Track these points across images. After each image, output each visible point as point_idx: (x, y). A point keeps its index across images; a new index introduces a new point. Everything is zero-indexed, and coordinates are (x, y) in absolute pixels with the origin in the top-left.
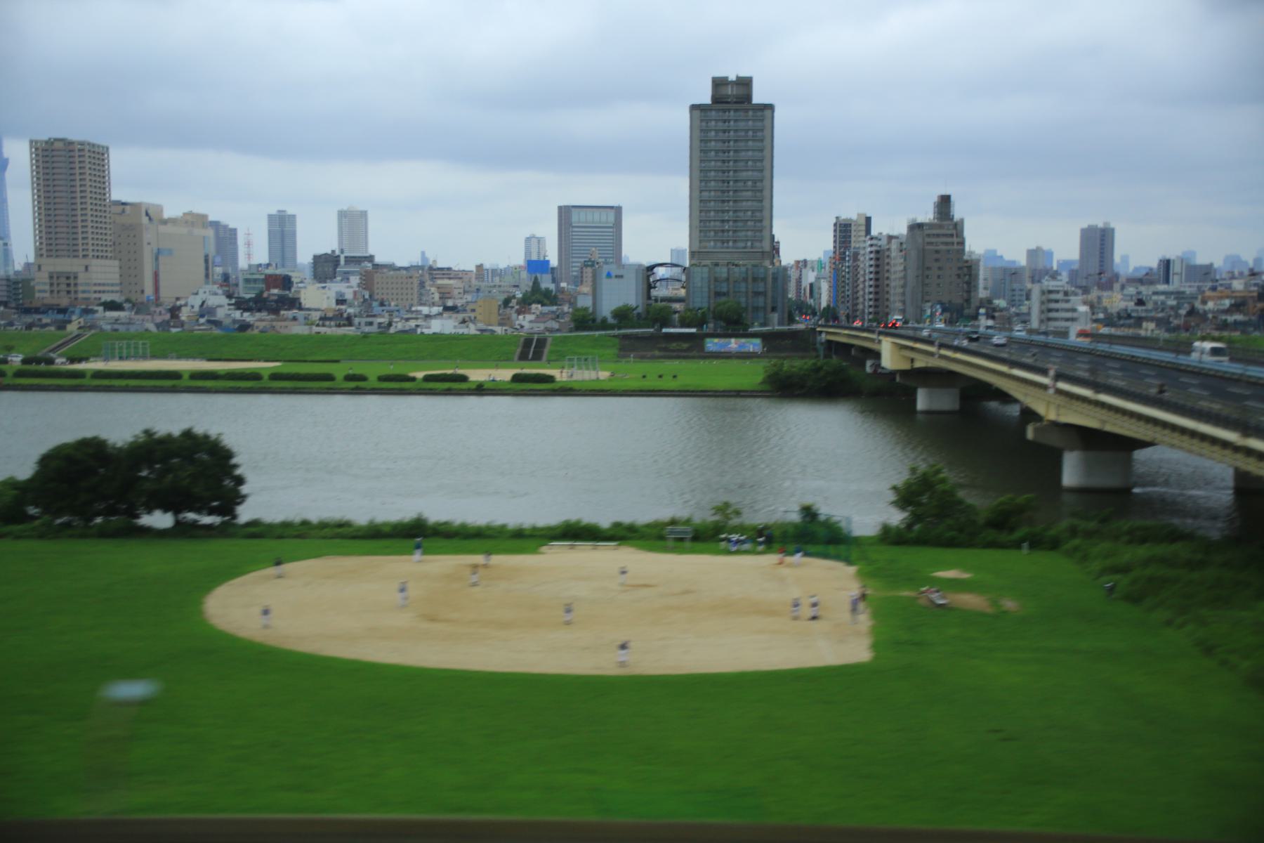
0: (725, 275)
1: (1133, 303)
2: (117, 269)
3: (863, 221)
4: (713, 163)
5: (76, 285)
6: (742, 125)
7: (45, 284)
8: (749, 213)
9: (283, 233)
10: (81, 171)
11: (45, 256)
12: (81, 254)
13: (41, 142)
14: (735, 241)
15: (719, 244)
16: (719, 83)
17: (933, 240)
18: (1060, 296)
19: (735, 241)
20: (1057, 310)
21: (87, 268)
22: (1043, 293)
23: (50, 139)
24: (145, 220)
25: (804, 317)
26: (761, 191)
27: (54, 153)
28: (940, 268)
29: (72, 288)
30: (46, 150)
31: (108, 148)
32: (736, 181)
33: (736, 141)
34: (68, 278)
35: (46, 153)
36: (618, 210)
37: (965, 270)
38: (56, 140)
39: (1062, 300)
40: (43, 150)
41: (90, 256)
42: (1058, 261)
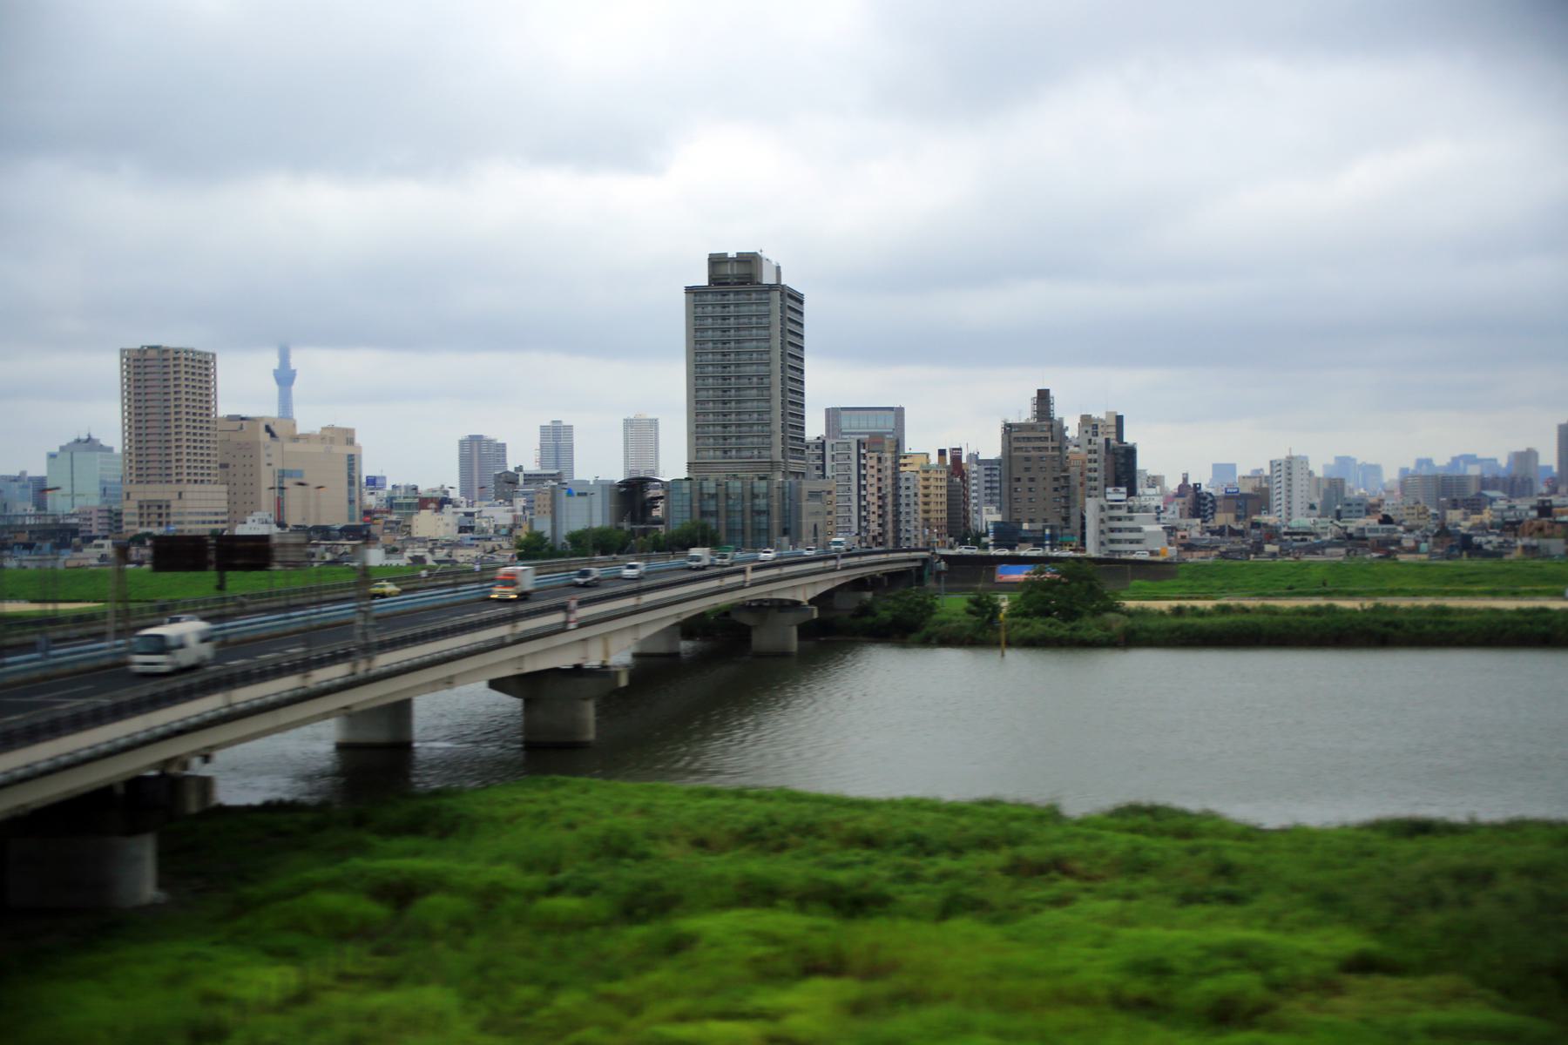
0: (764, 490)
1: (1376, 521)
2: (225, 496)
3: (1113, 422)
4: (710, 356)
5: (168, 515)
6: (744, 310)
7: (134, 514)
8: (755, 416)
9: (557, 448)
10: (176, 383)
11: (134, 482)
12: (174, 478)
13: (133, 350)
14: (739, 450)
15: (718, 453)
16: (716, 261)
17: (1023, 445)
18: (1123, 513)
19: (739, 450)
20: (1120, 530)
21: (180, 494)
22: (1102, 509)
23: (143, 347)
24: (265, 437)
25: (952, 539)
26: (768, 388)
27: (147, 363)
28: (1032, 480)
29: (164, 519)
30: (139, 360)
31: (214, 355)
32: (739, 377)
33: (738, 329)
34: (160, 507)
35: (137, 364)
36: (899, 412)
37: (1062, 481)
38: (150, 348)
39: (1126, 518)
40: (135, 360)
41: (185, 481)
42: (367, 477)
